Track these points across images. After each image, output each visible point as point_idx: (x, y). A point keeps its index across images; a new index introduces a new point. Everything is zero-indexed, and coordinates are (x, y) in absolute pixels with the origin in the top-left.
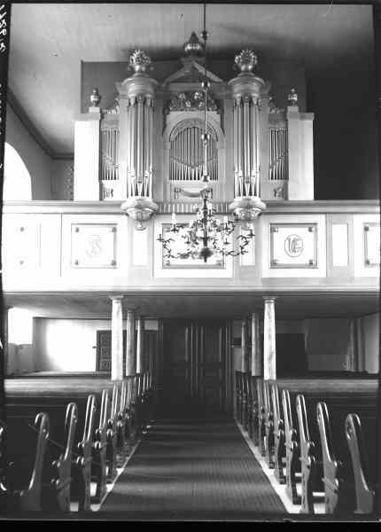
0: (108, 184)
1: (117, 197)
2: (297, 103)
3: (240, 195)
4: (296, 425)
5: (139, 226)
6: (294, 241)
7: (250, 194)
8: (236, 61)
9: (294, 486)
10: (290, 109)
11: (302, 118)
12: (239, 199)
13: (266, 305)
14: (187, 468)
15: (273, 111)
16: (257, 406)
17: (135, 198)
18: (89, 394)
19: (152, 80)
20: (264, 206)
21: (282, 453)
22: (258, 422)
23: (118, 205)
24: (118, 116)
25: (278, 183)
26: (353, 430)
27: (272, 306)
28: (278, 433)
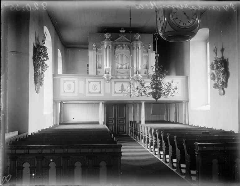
0: (98, 69)
1: (101, 74)
4: (151, 135)
5: (107, 82)
8: (105, 35)
9: (151, 149)
10: (149, 50)
11: (152, 52)
12: (105, 75)
14: (133, 147)
15: (144, 50)
16: (139, 131)
18: (157, 129)
19: (111, 41)
20: (142, 77)
21: (148, 142)
22: (140, 136)
23: (102, 76)
24: (101, 50)
25: (146, 70)
26: (168, 136)
28: (147, 137)
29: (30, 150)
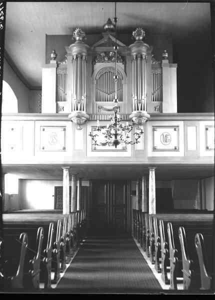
0: (61, 104)
1: (66, 111)
2: (168, 58)
3: (135, 110)
4: (167, 240)
5: (79, 127)
6: (166, 136)
7: (141, 109)
8: (133, 34)
9: (166, 274)
10: (164, 61)
11: (171, 66)
12: (135, 112)
13: (150, 172)
14: (106, 264)
15: (154, 63)
16: (145, 229)
17: (76, 111)
18: (50, 222)
19: (86, 45)
20: (149, 116)
21: (159, 256)
22: (145, 238)
23: (67, 115)
24: (66, 65)
25: (157, 103)
26: (199, 242)
27: (154, 172)
28: (157, 244)
29: (173, 288)
